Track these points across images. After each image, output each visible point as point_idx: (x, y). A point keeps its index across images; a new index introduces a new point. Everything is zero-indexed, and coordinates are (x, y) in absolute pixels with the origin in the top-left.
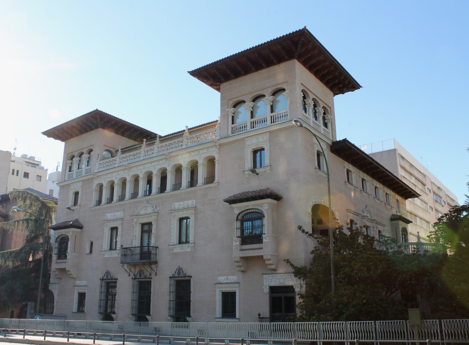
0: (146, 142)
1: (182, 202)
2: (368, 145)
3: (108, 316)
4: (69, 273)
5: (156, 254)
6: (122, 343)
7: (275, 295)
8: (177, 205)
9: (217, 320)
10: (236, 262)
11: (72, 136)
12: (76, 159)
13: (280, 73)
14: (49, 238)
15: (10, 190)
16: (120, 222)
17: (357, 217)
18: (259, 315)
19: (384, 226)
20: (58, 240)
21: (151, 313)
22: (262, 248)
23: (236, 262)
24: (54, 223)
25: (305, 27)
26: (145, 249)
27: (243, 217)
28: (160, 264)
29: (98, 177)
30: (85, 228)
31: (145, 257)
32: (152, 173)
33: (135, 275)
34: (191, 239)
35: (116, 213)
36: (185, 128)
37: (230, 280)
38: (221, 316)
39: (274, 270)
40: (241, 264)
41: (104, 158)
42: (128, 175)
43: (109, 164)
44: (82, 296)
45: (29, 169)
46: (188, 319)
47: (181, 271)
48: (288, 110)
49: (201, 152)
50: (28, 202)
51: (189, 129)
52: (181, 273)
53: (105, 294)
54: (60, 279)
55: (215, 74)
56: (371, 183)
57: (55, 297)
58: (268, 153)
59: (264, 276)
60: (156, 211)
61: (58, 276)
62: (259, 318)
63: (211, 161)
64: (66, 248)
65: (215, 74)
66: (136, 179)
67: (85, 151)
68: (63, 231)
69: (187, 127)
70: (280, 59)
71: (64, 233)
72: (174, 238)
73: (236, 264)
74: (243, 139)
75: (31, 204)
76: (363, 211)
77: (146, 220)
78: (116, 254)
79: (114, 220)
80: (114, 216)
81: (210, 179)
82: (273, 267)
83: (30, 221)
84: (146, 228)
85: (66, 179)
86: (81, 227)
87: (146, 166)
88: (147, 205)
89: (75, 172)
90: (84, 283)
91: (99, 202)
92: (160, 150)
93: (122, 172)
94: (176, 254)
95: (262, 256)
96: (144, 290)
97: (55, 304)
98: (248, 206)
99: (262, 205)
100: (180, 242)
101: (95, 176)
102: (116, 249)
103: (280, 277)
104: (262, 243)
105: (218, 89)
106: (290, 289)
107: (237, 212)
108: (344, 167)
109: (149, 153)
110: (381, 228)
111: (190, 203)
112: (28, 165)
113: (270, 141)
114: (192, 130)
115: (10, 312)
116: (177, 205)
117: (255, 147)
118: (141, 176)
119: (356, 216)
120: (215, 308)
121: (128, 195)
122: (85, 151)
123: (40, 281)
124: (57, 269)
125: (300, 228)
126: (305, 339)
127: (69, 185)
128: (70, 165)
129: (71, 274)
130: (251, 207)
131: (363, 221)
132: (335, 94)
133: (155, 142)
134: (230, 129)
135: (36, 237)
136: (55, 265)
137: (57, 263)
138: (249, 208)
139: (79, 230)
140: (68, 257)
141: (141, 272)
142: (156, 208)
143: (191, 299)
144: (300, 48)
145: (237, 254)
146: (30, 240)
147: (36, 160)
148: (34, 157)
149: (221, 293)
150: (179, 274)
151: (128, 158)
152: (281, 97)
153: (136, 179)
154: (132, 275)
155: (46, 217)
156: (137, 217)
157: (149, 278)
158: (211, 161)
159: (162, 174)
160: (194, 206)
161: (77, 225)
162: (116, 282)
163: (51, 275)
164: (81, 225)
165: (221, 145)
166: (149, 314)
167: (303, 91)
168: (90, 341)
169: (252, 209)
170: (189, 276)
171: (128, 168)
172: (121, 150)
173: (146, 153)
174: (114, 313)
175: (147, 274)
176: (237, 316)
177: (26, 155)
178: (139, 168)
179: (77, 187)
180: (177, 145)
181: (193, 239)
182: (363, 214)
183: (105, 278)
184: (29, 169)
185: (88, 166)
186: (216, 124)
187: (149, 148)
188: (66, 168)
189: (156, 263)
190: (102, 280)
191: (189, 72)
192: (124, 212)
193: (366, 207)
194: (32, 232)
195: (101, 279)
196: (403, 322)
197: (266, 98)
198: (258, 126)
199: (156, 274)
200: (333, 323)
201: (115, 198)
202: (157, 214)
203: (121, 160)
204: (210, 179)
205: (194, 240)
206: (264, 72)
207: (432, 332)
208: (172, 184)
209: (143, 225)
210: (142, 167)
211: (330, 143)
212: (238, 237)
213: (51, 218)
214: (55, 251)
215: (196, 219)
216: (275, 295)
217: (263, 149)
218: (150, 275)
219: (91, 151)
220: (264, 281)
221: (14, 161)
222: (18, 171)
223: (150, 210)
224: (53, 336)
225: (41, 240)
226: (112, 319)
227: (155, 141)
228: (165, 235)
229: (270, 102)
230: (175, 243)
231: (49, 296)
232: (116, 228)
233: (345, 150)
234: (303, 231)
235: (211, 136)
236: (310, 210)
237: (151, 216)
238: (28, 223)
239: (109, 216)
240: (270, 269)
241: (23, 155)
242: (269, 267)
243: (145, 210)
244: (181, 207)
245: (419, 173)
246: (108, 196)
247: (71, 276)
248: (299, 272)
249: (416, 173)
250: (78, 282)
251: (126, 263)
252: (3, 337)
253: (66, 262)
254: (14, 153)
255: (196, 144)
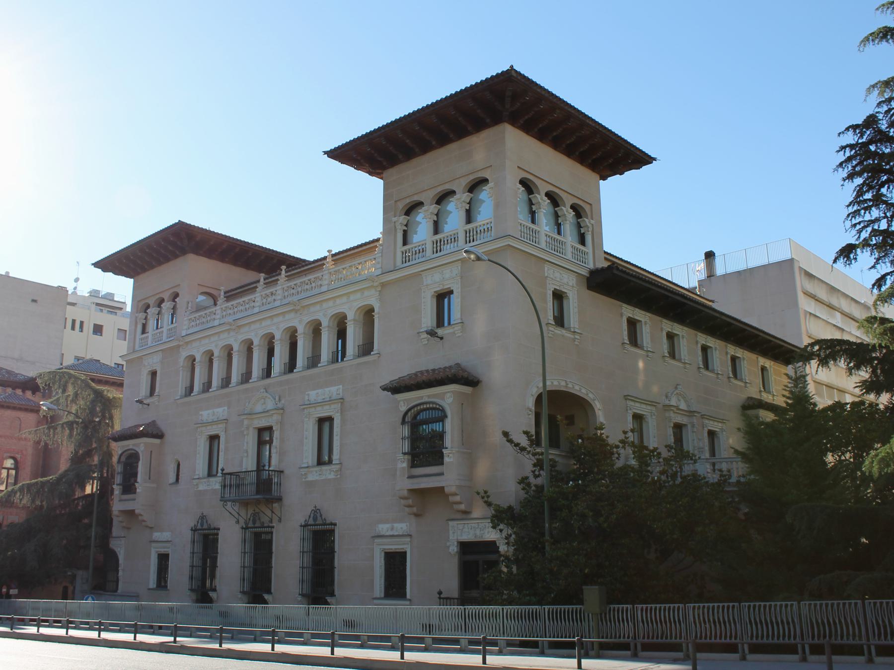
0: (286, 272)
1: (321, 392)
2: (682, 271)
3: (203, 594)
4: (140, 518)
5: (279, 484)
6: (172, 639)
7: (469, 558)
8: (313, 395)
9: (375, 601)
10: (401, 498)
11: (144, 270)
12: (152, 311)
13: (477, 151)
14: (110, 455)
15: (69, 361)
16: (338, 406)
17: (654, 409)
18: (440, 593)
19: (722, 421)
20: (123, 459)
21: (272, 591)
22: (442, 474)
23: (401, 498)
24: (118, 427)
25: (512, 67)
26: (265, 475)
27: (415, 417)
28: (286, 501)
29: (187, 343)
30: (168, 437)
31: (261, 490)
32: (345, 317)
33: (246, 523)
34: (336, 457)
35: (216, 410)
36: (327, 254)
37: (397, 529)
38: (383, 595)
39: (466, 512)
40: (410, 502)
41: (199, 308)
42: (236, 340)
43: (204, 320)
44: (163, 559)
45: (103, 318)
46: (329, 599)
47: (318, 515)
48: (492, 220)
49: (352, 297)
50: (71, 390)
51: (333, 255)
52: (319, 518)
53: (201, 555)
54: (129, 529)
55: (371, 153)
56: (690, 341)
57: (121, 561)
58: (459, 300)
59: (451, 523)
60: (280, 405)
61: (124, 524)
62: (440, 598)
63: (368, 314)
64: (135, 475)
65: (371, 153)
66: (316, 330)
67: (166, 296)
68: (130, 444)
69: (329, 251)
70: (479, 125)
71: (131, 447)
72: (310, 455)
73: (403, 502)
74: (418, 274)
75: (76, 395)
76: (667, 397)
77: (263, 423)
78: (215, 483)
79: (213, 423)
80: (214, 414)
81: (367, 348)
82: (462, 507)
83: (75, 426)
84: (264, 436)
85: (137, 348)
86: (160, 436)
87: (264, 324)
88: (266, 394)
89: (165, 330)
90: (166, 535)
91: (191, 389)
92: (286, 294)
93: (225, 335)
94: (311, 484)
95: (443, 488)
96: (261, 548)
97: (120, 573)
98: (422, 397)
99: (442, 396)
100: (320, 462)
101: (181, 343)
102: (330, 462)
103: (476, 526)
104: (442, 464)
105: (382, 178)
106: (491, 546)
107: (404, 408)
108: (622, 315)
109: (269, 299)
110: (715, 426)
111: (334, 391)
112: (101, 311)
113: (462, 278)
114: (340, 257)
115: (61, 589)
116: (313, 395)
117: (439, 288)
118: (325, 323)
119: (649, 407)
120: (373, 581)
121: (235, 378)
122: (166, 296)
123: (93, 534)
124: (120, 511)
125: (506, 434)
126: (611, 638)
127: (140, 358)
128: (144, 322)
129: (144, 521)
130: (426, 400)
131: (667, 415)
132: (604, 178)
133: (278, 280)
134: (399, 255)
135: (89, 453)
136: (118, 505)
137: (120, 500)
138: (423, 401)
139: (157, 441)
140: (138, 490)
141: (255, 516)
142: (280, 400)
143: (336, 564)
144: (508, 102)
145: (404, 484)
146: (77, 460)
147: (116, 299)
148: (112, 295)
149: (383, 554)
150: (315, 519)
151: (247, 306)
152: (485, 194)
153: (316, 330)
154: (242, 521)
155: (104, 417)
156: (249, 417)
157: (269, 527)
158: (368, 314)
159: (290, 339)
160: (340, 397)
161: (154, 432)
162: (217, 534)
163: (114, 524)
164: (161, 431)
165: (383, 285)
166: (269, 592)
167: (524, 183)
168: (475, 660)
169: (426, 403)
170: (332, 524)
171: (233, 327)
172: (225, 293)
173: (264, 301)
174: (215, 590)
175: (265, 520)
176: (408, 596)
177: (97, 292)
178: (253, 327)
179: (154, 362)
180: (300, 289)
181: (338, 457)
182: (667, 402)
183: (199, 527)
184: (103, 318)
185: (172, 323)
186: (376, 247)
187: (268, 291)
188: (136, 326)
189: (279, 499)
190: (194, 530)
191: (325, 153)
192: (229, 408)
193: (676, 388)
194: (79, 445)
195: (192, 530)
196: (856, 604)
197: (457, 196)
198: (447, 248)
199: (280, 520)
200: (728, 607)
201: (300, 361)
202: (281, 411)
203: (286, 294)
204: (367, 348)
205: (340, 459)
206: (453, 149)
207: (820, 621)
208: (357, 344)
209: (261, 431)
210: (257, 325)
211: (585, 273)
212: (405, 454)
213: (111, 418)
214: (118, 479)
215: (343, 421)
216: (469, 558)
217: (451, 292)
218: (271, 521)
219: (176, 295)
220: (451, 532)
221: (73, 304)
222: (82, 323)
223: (270, 405)
224: (362, 646)
225: (96, 460)
226: (210, 601)
227: (279, 277)
228: (295, 451)
229: (464, 204)
230: (310, 464)
231: (111, 558)
232: (330, 419)
233: (621, 283)
234: (510, 441)
235: (369, 267)
236: (531, 403)
237: (272, 415)
238: (71, 430)
239: (206, 415)
240: (459, 511)
241: (90, 292)
242: (456, 507)
243: (261, 402)
244: (320, 399)
245: (853, 304)
246: (286, 359)
247: (144, 523)
248: (500, 516)
249: (845, 305)
250: (157, 535)
251: (229, 501)
252: (217, 646)
253: (134, 500)
254: (75, 288)
255: (343, 283)
